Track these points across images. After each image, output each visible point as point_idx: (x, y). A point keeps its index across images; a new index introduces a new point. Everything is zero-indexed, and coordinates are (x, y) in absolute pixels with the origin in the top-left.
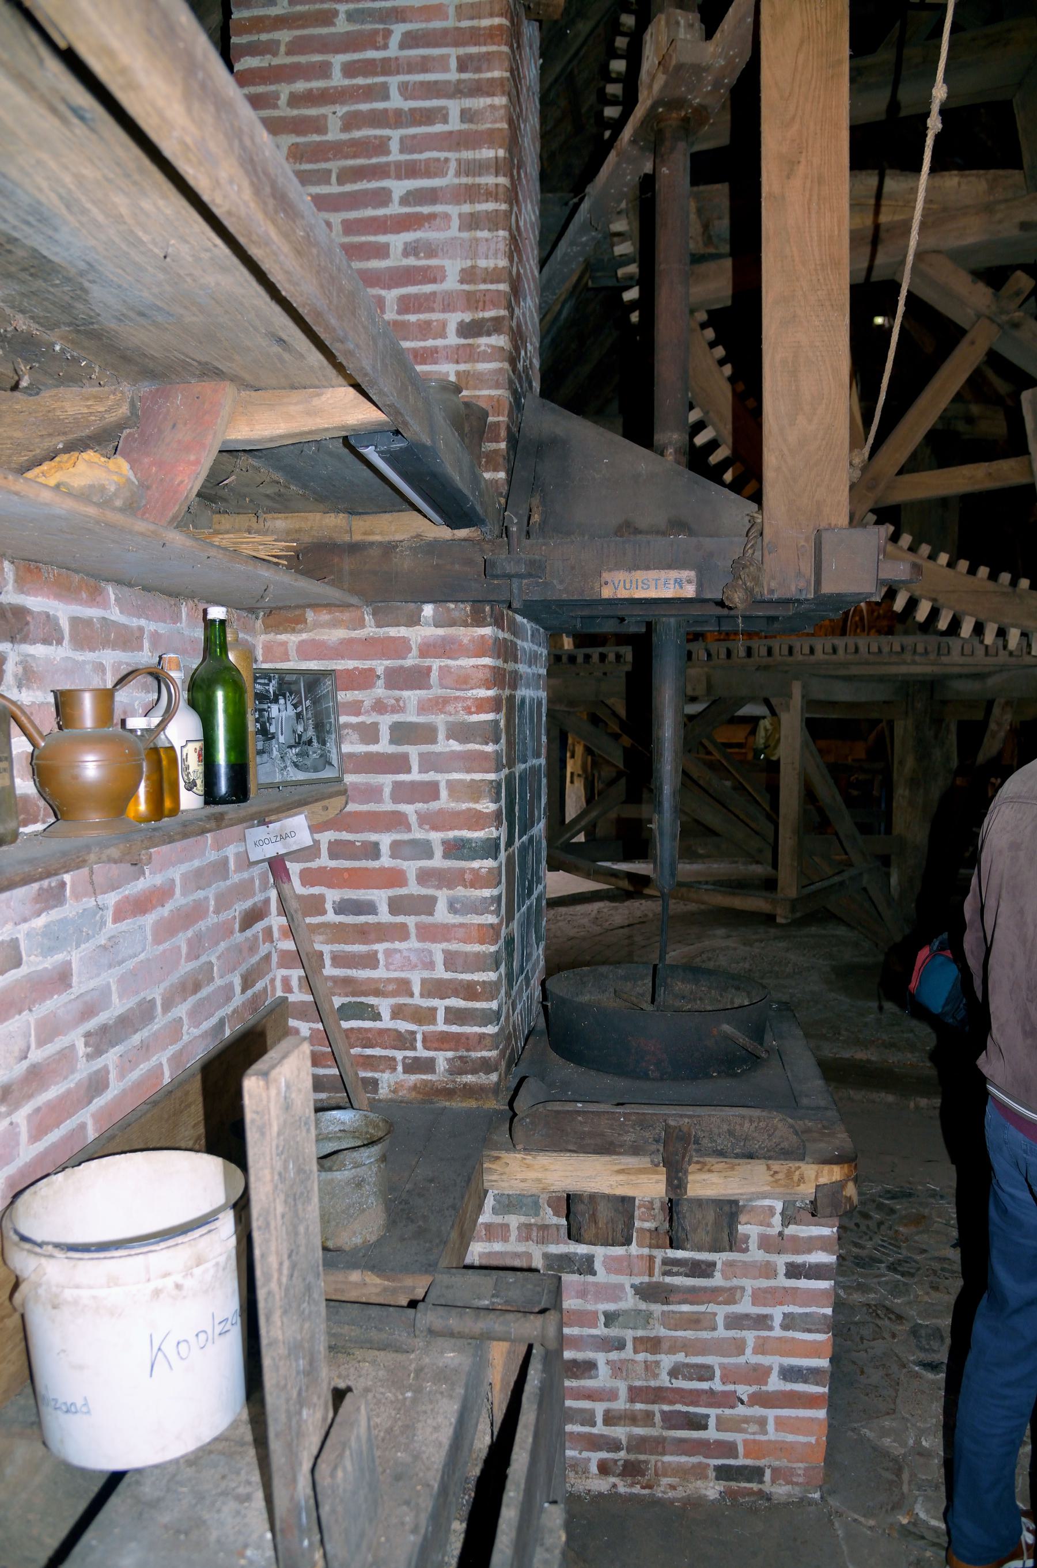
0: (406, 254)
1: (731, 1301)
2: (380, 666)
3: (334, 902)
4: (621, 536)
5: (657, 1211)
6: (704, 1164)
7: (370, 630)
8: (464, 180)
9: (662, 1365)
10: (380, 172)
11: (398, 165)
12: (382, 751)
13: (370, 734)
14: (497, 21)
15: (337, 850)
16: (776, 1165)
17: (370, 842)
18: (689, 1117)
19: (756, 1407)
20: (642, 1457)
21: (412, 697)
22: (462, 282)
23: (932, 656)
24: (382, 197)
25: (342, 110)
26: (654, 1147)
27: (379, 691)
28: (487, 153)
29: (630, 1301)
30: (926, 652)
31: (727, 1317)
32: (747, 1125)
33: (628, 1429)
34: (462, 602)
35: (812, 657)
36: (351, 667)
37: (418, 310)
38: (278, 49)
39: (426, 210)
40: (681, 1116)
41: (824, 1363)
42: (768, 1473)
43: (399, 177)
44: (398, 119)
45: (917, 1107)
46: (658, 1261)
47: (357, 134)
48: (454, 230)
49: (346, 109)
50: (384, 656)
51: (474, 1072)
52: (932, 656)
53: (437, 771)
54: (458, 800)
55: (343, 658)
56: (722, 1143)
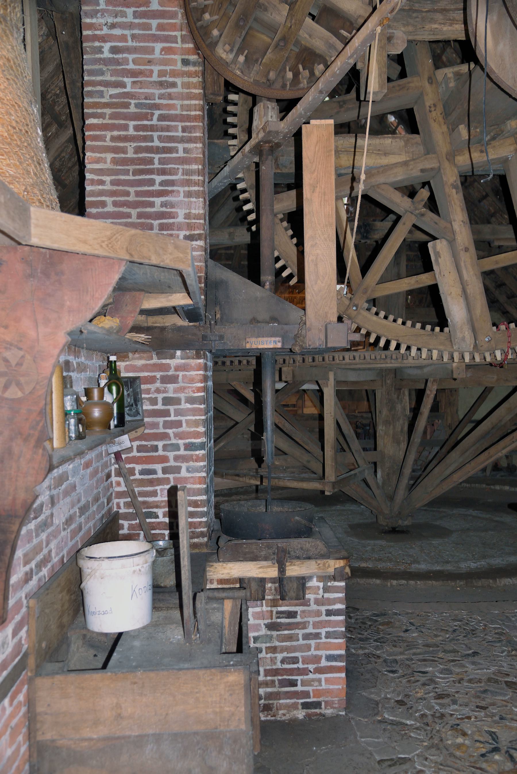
0: (162, 206)
1: (304, 628)
2: (158, 375)
3: (139, 470)
4: (252, 324)
5: (273, 591)
6: (292, 562)
7: (155, 360)
8: (185, 177)
9: (278, 658)
10: (151, 172)
11: (158, 169)
12: (159, 408)
13: (154, 401)
14: (198, 113)
15: (140, 449)
16: (319, 562)
17: (154, 445)
18: (286, 542)
19: (317, 674)
20: (271, 702)
21: (171, 387)
22: (185, 218)
23: (400, 360)
24: (152, 182)
25: (134, 145)
26: (272, 557)
27: (158, 384)
28: (195, 167)
29: (264, 631)
30: (397, 358)
31: (303, 635)
32: (307, 544)
33: (264, 689)
34: (192, 350)
35: (343, 361)
36: (146, 375)
37: (167, 230)
38: (105, 117)
39: (170, 188)
40: (283, 542)
41: (343, 652)
42: (323, 704)
43: (158, 175)
44: (157, 150)
45: (391, 585)
46: (274, 613)
47: (140, 155)
48: (181, 198)
49: (135, 144)
50: (161, 370)
51: (198, 537)
52: (400, 360)
53: (181, 416)
54: (190, 427)
55: (143, 372)
56: (299, 553)
